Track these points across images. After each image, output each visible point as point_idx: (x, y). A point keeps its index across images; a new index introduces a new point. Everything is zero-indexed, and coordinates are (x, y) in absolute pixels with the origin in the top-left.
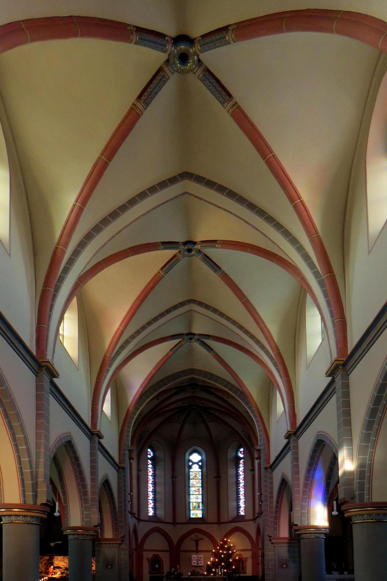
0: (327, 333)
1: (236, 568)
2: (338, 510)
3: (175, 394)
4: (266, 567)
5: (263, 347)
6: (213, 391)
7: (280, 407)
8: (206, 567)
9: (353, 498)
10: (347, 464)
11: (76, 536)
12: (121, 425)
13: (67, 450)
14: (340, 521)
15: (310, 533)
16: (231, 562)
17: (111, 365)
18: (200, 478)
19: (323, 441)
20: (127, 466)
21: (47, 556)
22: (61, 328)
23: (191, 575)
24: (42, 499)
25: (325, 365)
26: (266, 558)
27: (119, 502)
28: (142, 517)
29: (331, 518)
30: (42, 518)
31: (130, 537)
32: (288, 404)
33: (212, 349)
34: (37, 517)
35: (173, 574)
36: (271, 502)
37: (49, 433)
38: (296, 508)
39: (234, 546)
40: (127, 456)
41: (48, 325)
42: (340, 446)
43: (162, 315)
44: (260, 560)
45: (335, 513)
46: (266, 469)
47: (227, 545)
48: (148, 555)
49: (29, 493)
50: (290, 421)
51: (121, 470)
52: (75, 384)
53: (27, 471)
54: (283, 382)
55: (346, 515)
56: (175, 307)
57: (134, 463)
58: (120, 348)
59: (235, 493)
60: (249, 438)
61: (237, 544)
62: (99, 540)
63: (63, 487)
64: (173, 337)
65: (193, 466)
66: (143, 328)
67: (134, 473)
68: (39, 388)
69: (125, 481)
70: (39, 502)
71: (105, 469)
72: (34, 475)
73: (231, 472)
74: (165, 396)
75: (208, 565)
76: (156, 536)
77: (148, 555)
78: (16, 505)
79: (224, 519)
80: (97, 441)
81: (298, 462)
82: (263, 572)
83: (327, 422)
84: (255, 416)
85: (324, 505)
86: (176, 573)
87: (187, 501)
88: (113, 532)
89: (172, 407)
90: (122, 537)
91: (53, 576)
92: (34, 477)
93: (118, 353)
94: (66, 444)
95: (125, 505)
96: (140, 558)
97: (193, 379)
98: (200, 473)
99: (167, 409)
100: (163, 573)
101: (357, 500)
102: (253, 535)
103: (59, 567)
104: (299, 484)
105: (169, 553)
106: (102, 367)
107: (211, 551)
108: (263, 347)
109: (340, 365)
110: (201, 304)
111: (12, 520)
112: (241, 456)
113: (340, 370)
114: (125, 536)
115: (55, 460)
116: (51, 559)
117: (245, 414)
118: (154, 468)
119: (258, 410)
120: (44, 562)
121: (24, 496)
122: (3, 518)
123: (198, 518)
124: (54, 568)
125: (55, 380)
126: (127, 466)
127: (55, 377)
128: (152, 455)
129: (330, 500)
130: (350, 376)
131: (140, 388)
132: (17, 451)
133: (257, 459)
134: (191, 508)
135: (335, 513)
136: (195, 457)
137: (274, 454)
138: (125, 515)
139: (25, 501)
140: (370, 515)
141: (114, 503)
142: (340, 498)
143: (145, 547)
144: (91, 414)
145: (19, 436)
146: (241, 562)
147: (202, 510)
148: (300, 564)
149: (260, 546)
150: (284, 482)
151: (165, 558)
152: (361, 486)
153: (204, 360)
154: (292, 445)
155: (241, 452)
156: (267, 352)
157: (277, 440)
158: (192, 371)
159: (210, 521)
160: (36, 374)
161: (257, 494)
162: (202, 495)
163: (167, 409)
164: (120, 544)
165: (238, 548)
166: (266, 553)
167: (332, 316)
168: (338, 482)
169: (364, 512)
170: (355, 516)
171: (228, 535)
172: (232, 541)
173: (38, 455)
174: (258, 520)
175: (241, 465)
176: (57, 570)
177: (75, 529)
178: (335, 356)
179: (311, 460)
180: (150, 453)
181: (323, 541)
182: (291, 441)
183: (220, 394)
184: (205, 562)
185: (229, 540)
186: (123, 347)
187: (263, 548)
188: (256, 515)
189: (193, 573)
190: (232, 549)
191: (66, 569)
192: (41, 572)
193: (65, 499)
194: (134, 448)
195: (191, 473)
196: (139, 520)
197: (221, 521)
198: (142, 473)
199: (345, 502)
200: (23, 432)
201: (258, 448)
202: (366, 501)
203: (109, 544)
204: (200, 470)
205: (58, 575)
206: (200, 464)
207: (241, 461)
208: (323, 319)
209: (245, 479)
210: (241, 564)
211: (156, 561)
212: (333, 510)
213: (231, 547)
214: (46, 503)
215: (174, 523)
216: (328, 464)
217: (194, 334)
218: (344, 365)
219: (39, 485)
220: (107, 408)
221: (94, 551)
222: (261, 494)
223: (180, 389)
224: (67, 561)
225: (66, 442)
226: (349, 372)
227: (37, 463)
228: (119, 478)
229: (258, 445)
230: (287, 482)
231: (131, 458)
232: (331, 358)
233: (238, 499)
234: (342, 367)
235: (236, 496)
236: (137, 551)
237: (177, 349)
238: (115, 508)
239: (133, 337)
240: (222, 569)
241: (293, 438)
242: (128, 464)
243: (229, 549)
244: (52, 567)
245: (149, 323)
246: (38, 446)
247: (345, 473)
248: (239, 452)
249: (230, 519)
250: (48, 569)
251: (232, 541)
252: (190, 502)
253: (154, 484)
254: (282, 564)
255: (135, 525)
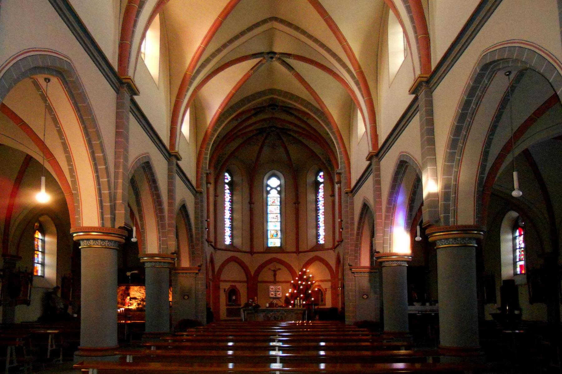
0: (410, 50)
1: (315, 299)
2: (423, 234)
3: (255, 115)
4: (346, 298)
5: (344, 65)
6: (293, 112)
7: (361, 128)
8: (284, 299)
9: (438, 221)
10: (431, 186)
11: (153, 264)
12: (199, 147)
13: (145, 172)
14: (423, 247)
15: (392, 261)
16: (310, 294)
17: (191, 83)
18: (279, 204)
19: (406, 162)
20: (204, 190)
21: (123, 286)
22: (143, 46)
23: (269, 307)
24: (120, 223)
25: (408, 82)
26: (346, 288)
27: (197, 228)
28: (219, 246)
29: (414, 244)
30: (119, 242)
31: (206, 266)
32: (370, 124)
33: (293, 69)
34: (115, 241)
35: (251, 305)
36: (352, 229)
37: (127, 152)
38: (379, 235)
39: (313, 277)
40: (205, 179)
41: (131, 42)
42: (425, 165)
43: (243, 33)
44: (340, 291)
45: (418, 238)
46: (347, 193)
47: (306, 275)
48: (224, 286)
49: (108, 216)
50: (372, 141)
51: (198, 195)
52: (155, 102)
53: (106, 192)
54: (365, 101)
55: (430, 239)
56: (257, 25)
57: (211, 187)
58: (200, 67)
59: (314, 221)
60: (329, 161)
61: (316, 274)
62: (176, 269)
63: (140, 211)
64: (255, 56)
65: (271, 192)
66: (225, 46)
67: (212, 199)
68: (119, 105)
69: (202, 206)
70: (117, 226)
71: (183, 194)
72: (113, 198)
73: (311, 197)
74: (244, 117)
75: (286, 297)
76: (233, 266)
77: (224, 286)
78: (95, 228)
79: (302, 248)
80: (175, 163)
81: (380, 185)
82: (343, 304)
83: (410, 143)
84: (336, 139)
85: (407, 231)
86: (254, 305)
87: (265, 230)
88: (190, 261)
89: (251, 129)
90: (199, 266)
91: (130, 307)
92: (113, 198)
93: (198, 72)
94: (144, 165)
95: (202, 232)
96: (217, 288)
97: (272, 99)
98: (279, 199)
99: (247, 130)
100: (240, 305)
101: (442, 224)
102: (333, 263)
103: (135, 298)
104: (381, 209)
105: (246, 284)
106: (182, 86)
107: (289, 282)
108: (344, 65)
109: (423, 81)
110: (282, 21)
111: (91, 245)
112: (321, 180)
113: (423, 88)
114: (201, 264)
115: (133, 183)
116: (128, 289)
117: (324, 135)
118: (232, 194)
119: (338, 130)
120: (121, 292)
121: (102, 219)
122: (82, 243)
123: (276, 247)
124: (131, 299)
125: (136, 97)
126: (204, 190)
127: (136, 94)
128: (230, 180)
129: (413, 224)
130: (434, 94)
131: (219, 108)
132: (96, 171)
133: (337, 183)
134: (269, 237)
135: (418, 238)
136: (274, 182)
137: (355, 178)
138: (202, 243)
139: (103, 224)
140: (455, 239)
141: (190, 230)
142: (424, 221)
143: (223, 277)
144: (169, 135)
145: (99, 155)
146: (320, 293)
147: (281, 238)
148: (381, 293)
149: (340, 276)
150: (365, 207)
151: (243, 289)
152: (446, 209)
153: (284, 80)
154: (373, 167)
155: (320, 176)
156: (349, 71)
157: (358, 161)
158: (272, 91)
159: (288, 250)
160: (117, 91)
161: (338, 220)
162: (281, 222)
163: (247, 130)
164: (197, 273)
165: (317, 279)
166: (346, 283)
167: (415, 32)
168: (422, 204)
169: (451, 236)
170: (440, 240)
171: (307, 265)
172: (311, 271)
173: (116, 178)
174: (337, 250)
175: (320, 191)
176: (133, 301)
177: (152, 256)
178: (418, 73)
179: (393, 182)
180: (228, 178)
181: (406, 269)
182: (373, 163)
183: (300, 116)
184: (284, 293)
185: (308, 271)
186: (203, 66)
187: (343, 279)
188: (336, 243)
189: (271, 305)
190: (311, 279)
191: (143, 300)
192: (118, 303)
193: (143, 225)
194: (212, 171)
195: (269, 199)
196: (215, 248)
197: (300, 250)
198: (219, 199)
199: (429, 226)
200: (103, 151)
201: (338, 171)
202: (451, 224)
203: (186, 273)
204: (279, 196)
205: (134, 306)
206: (279, 189)
207: (321, 186)
208: (405, 32)
209: (325, 205)
210: (320, 295)
211: (233, 292)
212: (416, 236)
213: (310, 277)
214: (124, 227)
215: (252, 252)
216: (411, 187)
217: (275, 53)
218: (428, 82)
219: (118, 206)
220: (185, 129)
221: (170, 281)
222: (342, 221)
223: (259, 110)
224: (143, 291)
225: (144, 163)
226: (433, 88)
227: (116, 184)
228: (196, 203)
229: (338, 168)
230: (368, 207)
231: (208, 183)
232: (415, 75)
233: (317, 227)
234: (425, 84)
235: (315, 223)
236: (214, 282)
237: (258, 68)
238: (191, 236)
239: (213, 55)
240: (301, 301)
241: (374, 160)
242: (205, 188)
243: (307, 280)
244: (129, 298)
245: (231, 41)
246: (116, 166)
247: (429, 195)
248: (319, 177)
249: (309, 248)
250: (124, 300)
251: (311, 271)
252: (267, 230)
253: (232, 210)
254: (363, 294)
255: (211, 255)
